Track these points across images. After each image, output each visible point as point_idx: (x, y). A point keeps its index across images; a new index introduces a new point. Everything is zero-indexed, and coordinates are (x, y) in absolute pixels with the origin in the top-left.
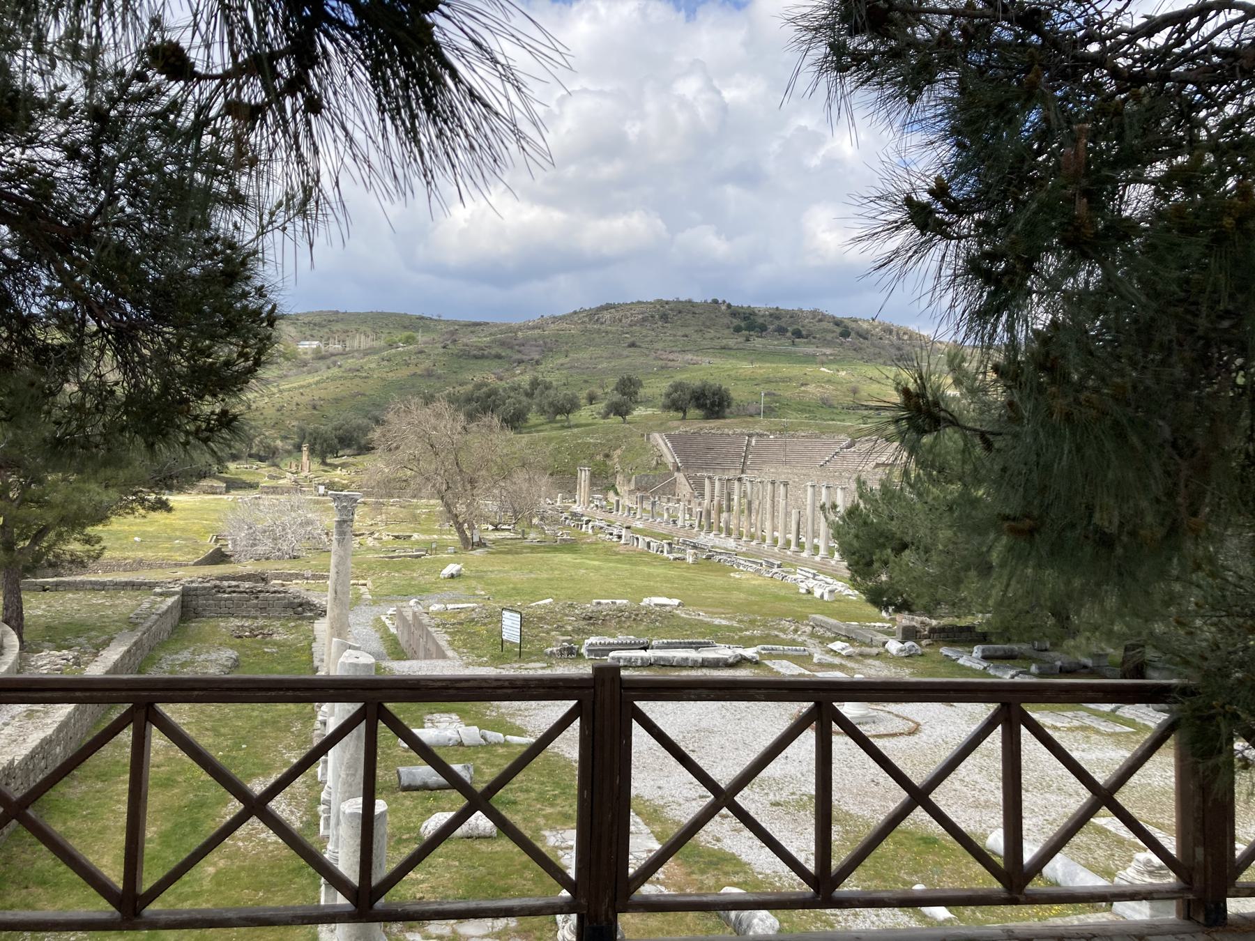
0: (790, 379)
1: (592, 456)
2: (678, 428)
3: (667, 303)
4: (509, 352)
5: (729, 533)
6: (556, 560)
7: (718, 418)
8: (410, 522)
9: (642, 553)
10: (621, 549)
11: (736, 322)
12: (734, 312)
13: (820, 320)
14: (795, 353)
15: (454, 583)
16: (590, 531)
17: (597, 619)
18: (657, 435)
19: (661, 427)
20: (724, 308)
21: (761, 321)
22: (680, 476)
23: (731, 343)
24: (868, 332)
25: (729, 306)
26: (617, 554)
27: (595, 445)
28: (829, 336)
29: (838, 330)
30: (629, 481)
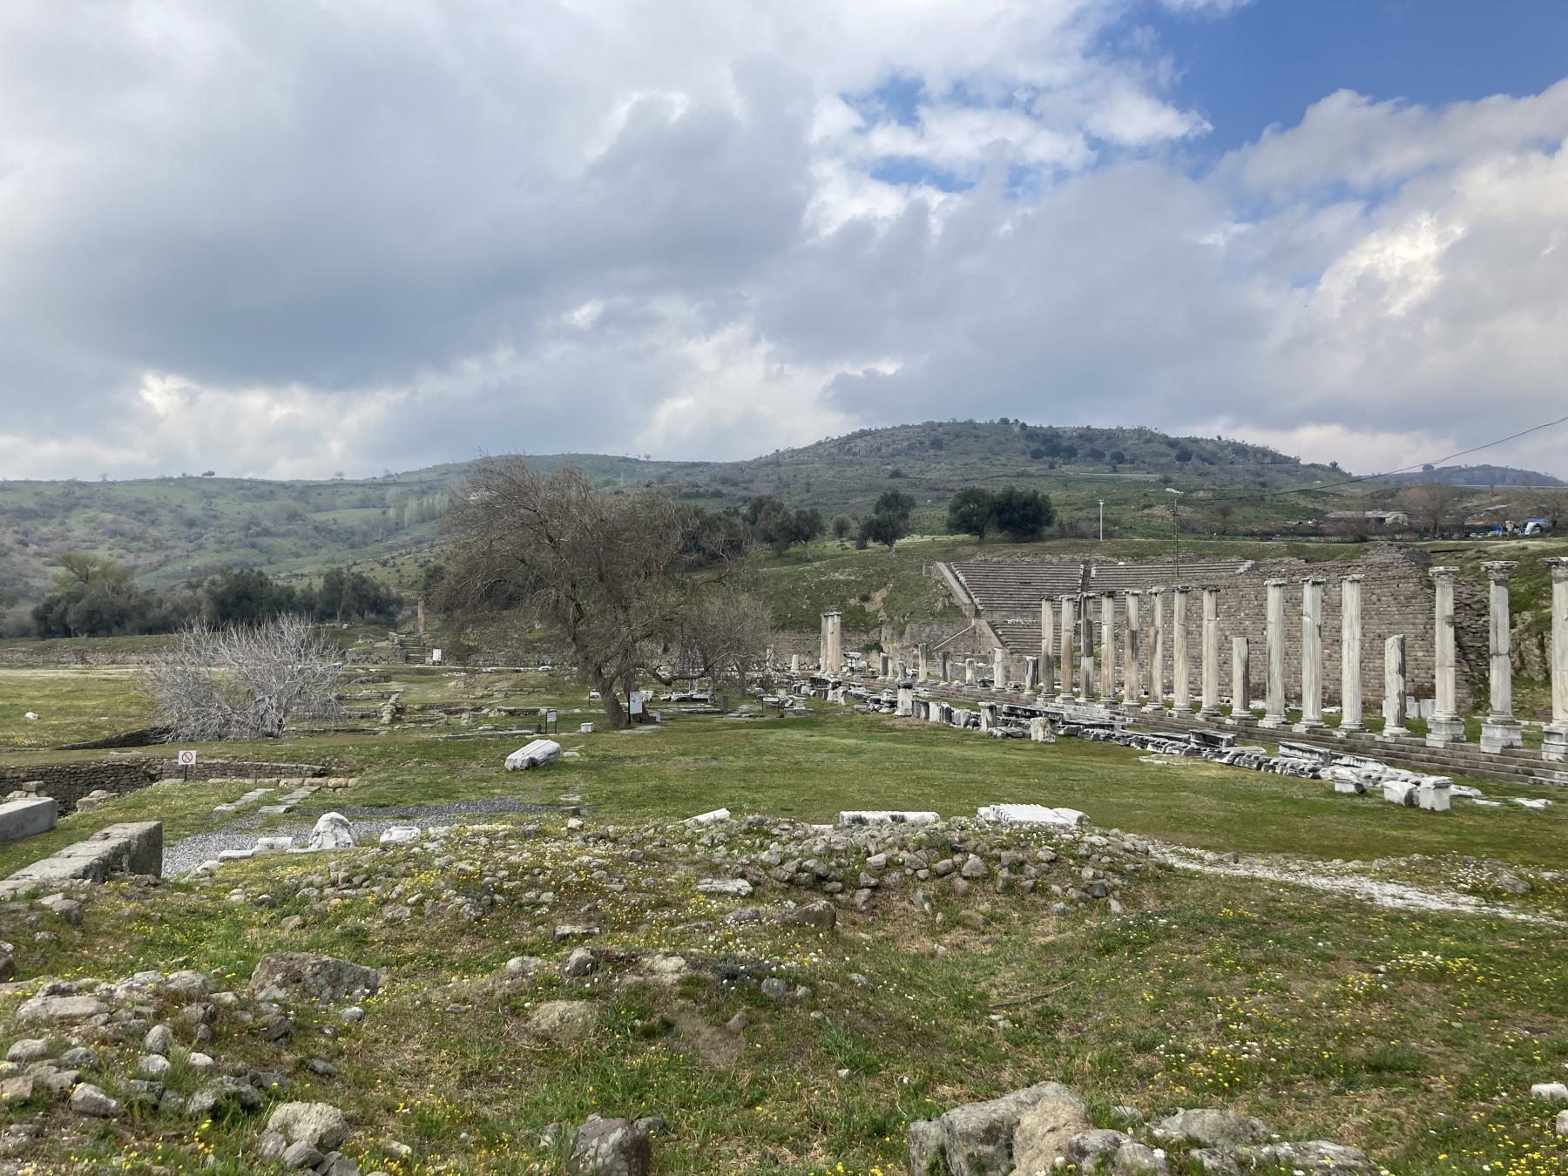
0: (1126, 501)
1: (843, 599)
2: (973, 555)
3: (940, 425)
4: (733, 489)
5: (1093, 697)
6: (772, 739)
7: (1033, 540)
8: (548, 692)
9: (936, 728)
10: (899, 724)
11: (1034, 446)
12: (1030, 434)
13: (1148, 441)
14: (1119, 479)
15: (529, 781)
16: (842, 701)
17: (851, 883)
18: (942, 566)
19: (949, 554)
20: (1017, 429)
21: (1066, 443)
22: (982, 624)
23: (1032, 470)
24: (1214, 455)
25: (1024, 426)
26: (891, 729)
27: (847, 583)
28: (1164, 461)
29: (1174, 453)
30: (902, 634)
